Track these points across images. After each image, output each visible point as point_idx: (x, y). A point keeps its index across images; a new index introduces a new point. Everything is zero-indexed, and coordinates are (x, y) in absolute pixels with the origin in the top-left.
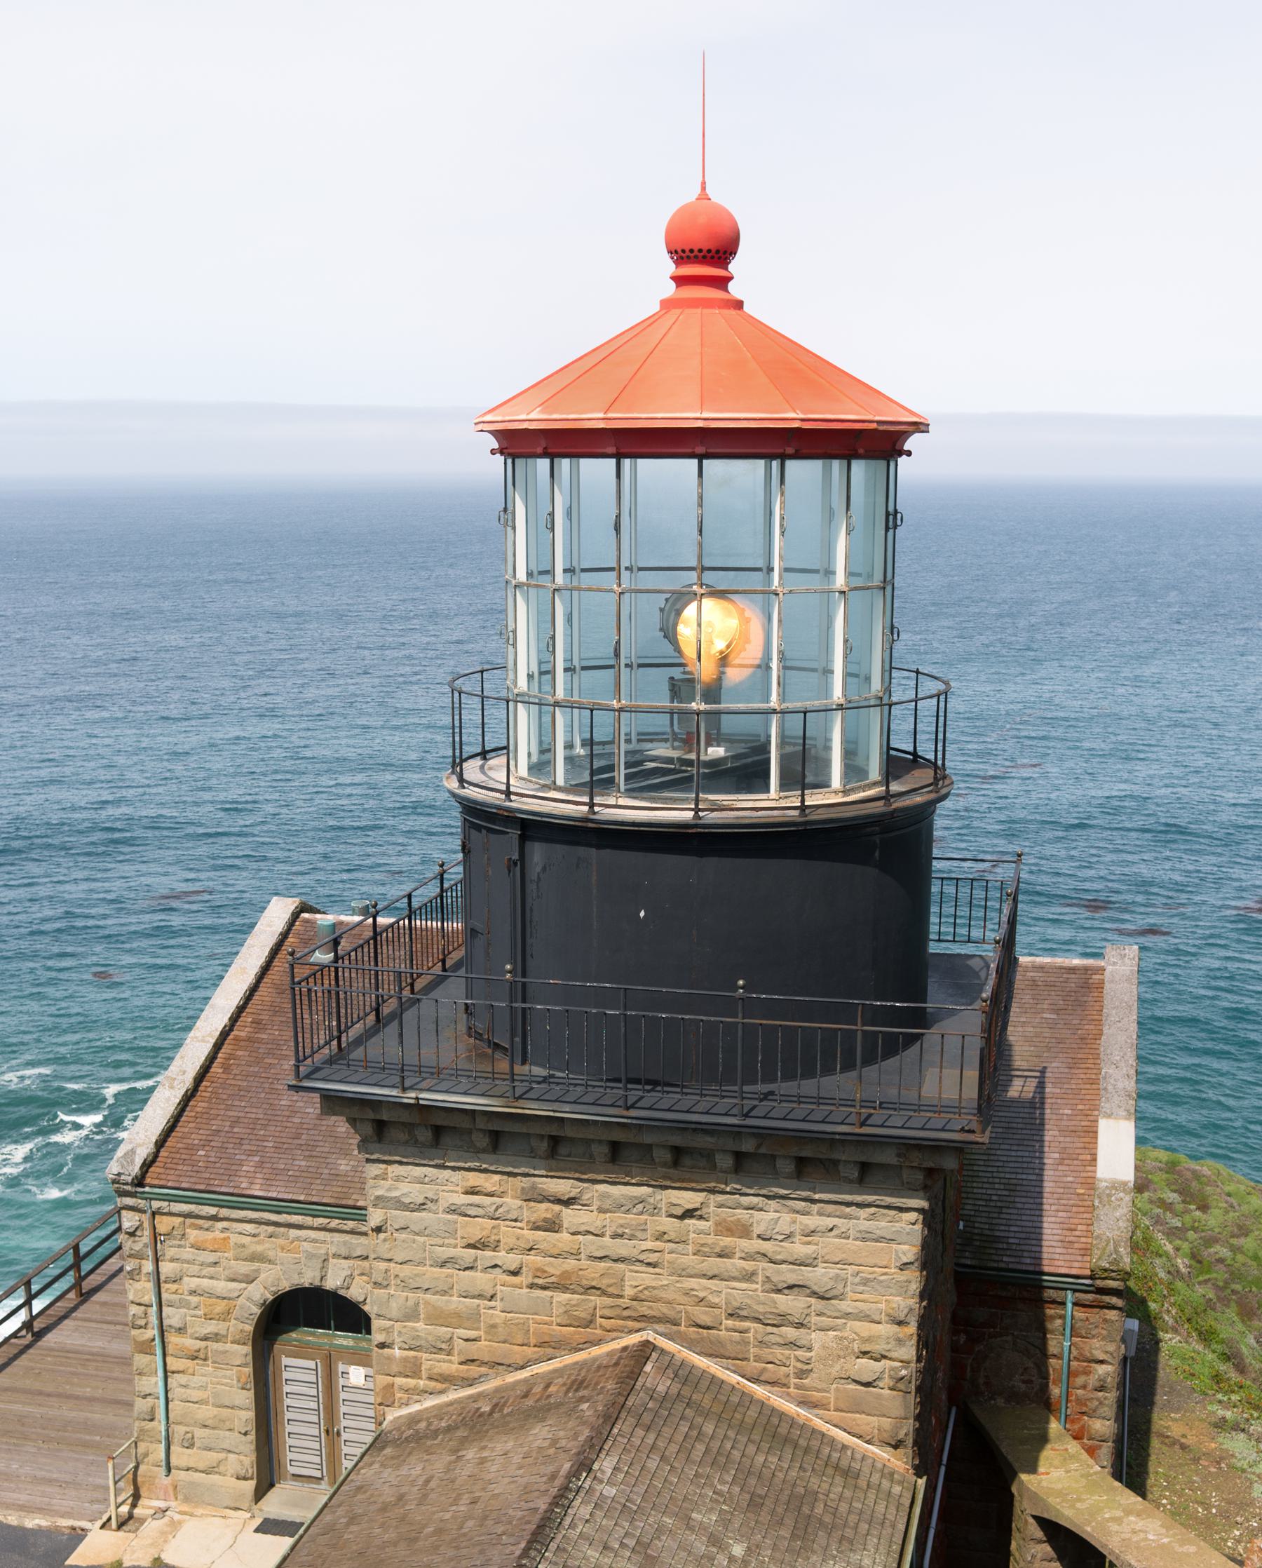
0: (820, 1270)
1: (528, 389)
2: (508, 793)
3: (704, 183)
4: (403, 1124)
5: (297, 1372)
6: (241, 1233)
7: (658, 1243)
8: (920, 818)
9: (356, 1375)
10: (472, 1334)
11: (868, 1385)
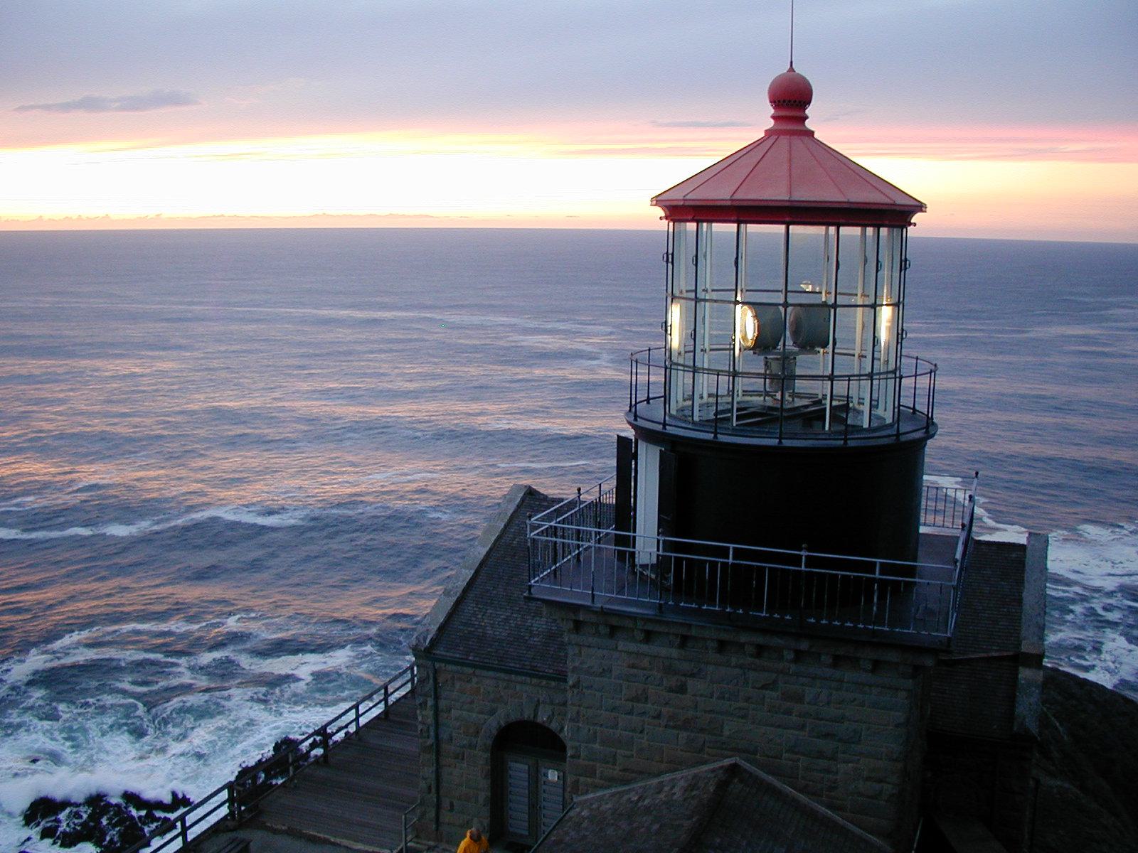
2: (665, 424)
3: (791, 63)
5: (518, 769)
8: (919, 445)
9: (553, 775)
10: (628, 753)
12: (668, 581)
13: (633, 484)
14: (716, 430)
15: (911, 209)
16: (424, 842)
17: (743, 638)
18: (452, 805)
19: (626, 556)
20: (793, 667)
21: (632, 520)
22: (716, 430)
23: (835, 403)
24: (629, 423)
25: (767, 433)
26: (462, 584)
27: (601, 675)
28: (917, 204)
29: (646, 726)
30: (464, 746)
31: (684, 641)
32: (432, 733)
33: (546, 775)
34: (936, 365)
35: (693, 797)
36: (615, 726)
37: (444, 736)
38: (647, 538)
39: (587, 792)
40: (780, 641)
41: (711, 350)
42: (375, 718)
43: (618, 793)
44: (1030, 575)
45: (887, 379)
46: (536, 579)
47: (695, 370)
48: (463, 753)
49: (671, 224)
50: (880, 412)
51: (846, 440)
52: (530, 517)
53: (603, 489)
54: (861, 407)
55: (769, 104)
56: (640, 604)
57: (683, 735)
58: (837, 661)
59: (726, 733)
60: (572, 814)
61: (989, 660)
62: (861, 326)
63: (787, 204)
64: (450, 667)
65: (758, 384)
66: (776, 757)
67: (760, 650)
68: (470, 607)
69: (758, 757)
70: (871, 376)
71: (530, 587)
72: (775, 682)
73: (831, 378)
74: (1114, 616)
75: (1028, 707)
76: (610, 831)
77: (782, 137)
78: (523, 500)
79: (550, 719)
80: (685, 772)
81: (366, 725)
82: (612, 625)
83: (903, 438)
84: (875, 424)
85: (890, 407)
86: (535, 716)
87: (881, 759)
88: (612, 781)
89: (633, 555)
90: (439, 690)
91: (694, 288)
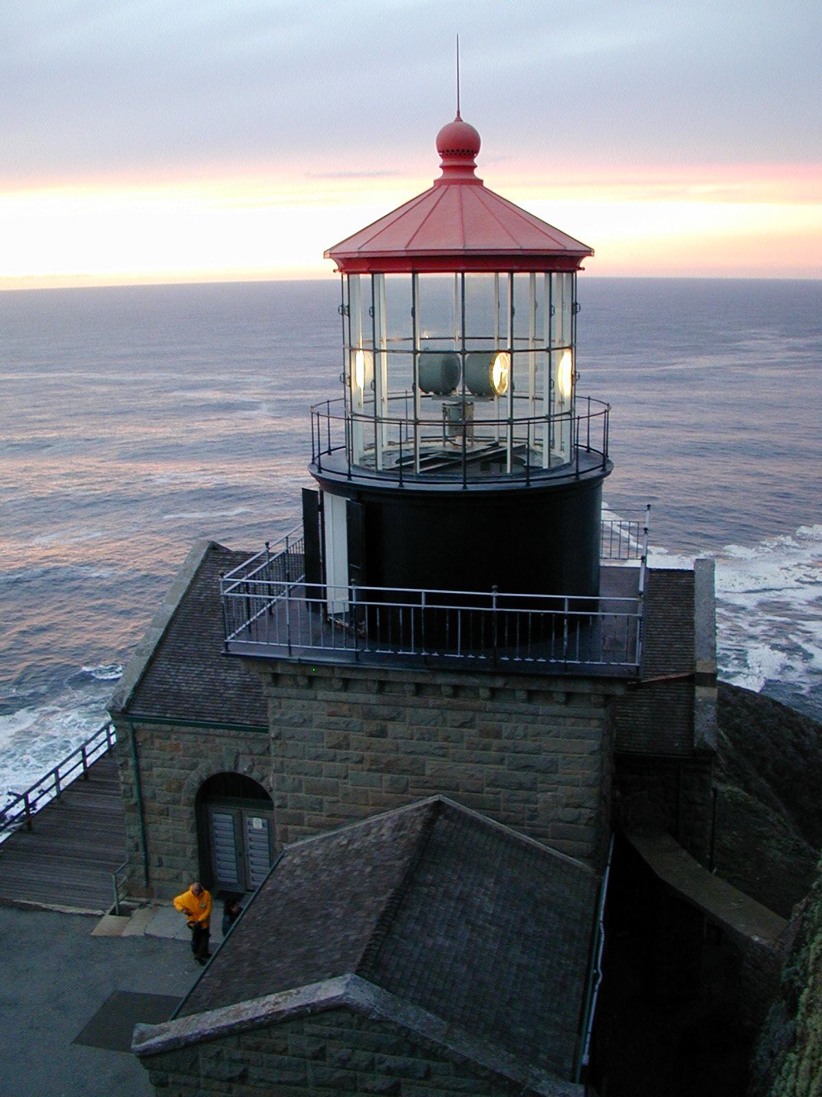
0: (543, 756)
1: (348, 239)
2: (349, 475)
3: (458, 112)
4: (290, 675)
5: (223, 821)
6: (187, 737)
7: (445, 743)
8: (595, 483)
9: (257, 823)
10: (335, 799)
11: (571, 822)
12: (361, 629)
13: (320, 532)
14: (401, 478)
15: (579, 254)
16: (135, 899)
17: (440, 680)
18: (160, 860)
19: (318, 609)
20: (489, 705)
21: (321, 567)
22: (401, 478)
23: (515, 445)
24: (313, 475)
25: (451, 478)
26: (153, 643)
27: (302, 725)
28: (587, 249)
29: (350, 772)
30: (168, 802)
31: (382, 686)
32: (135, 792)
33: (250, 824)
34: (608, 405)
35: (402, 837)
36: (319, 774)
37: (147, 793)
38: (338, 589)
39: (296, 840)
40: (477, 681)
41: (389, 399)
42: (75, 781)
43: (328, 838)
44: (700, 600)
45: (561, 420)
46: (233, 635)
47: (377, 420)
48: (168, 809)
49: (345, 277)
50: (556, 452)
51: (528, 481)
52: (222, 575)
53: (292, 539)
54: (538, 448)
55: (437, 154)
56: (337, 653)
57: (387, 777)
58: (531, 696)
59: (428, 772)
60: (283, 862)
61: (668, 682)
62: (533, 369)
63: (462, 253)
64: (148, 726)
65: (438, 431)
66: (478, 792)
67: (457, 690)
68: (163, 664)
69: (460, 793)
70: (549, 418)
71: (227, 644)
72: (472, 720)
73: (510, 422)
74: (756, 631)
75: (706, 724)
76: (324, 877)
77: (452, 186)
78: (207, 555)
79: (251, 769)
80: (392, 813)
81: (67, 788)
82: (310, 676)
83: (582, 477)
84: (553, 465)
85: (567, 448)
86: (236, 766)
87: (578, 786)
88: (320, 827)
89: (325, 605)
90: (138, 750)
91: (412, 336)
